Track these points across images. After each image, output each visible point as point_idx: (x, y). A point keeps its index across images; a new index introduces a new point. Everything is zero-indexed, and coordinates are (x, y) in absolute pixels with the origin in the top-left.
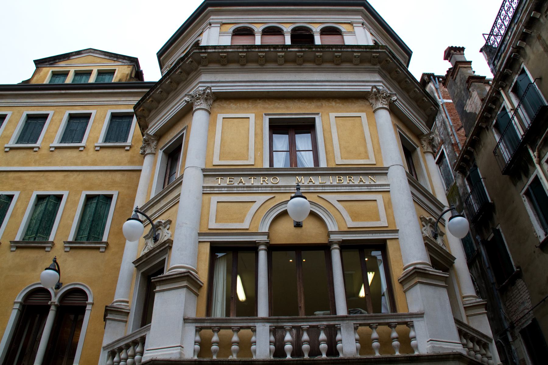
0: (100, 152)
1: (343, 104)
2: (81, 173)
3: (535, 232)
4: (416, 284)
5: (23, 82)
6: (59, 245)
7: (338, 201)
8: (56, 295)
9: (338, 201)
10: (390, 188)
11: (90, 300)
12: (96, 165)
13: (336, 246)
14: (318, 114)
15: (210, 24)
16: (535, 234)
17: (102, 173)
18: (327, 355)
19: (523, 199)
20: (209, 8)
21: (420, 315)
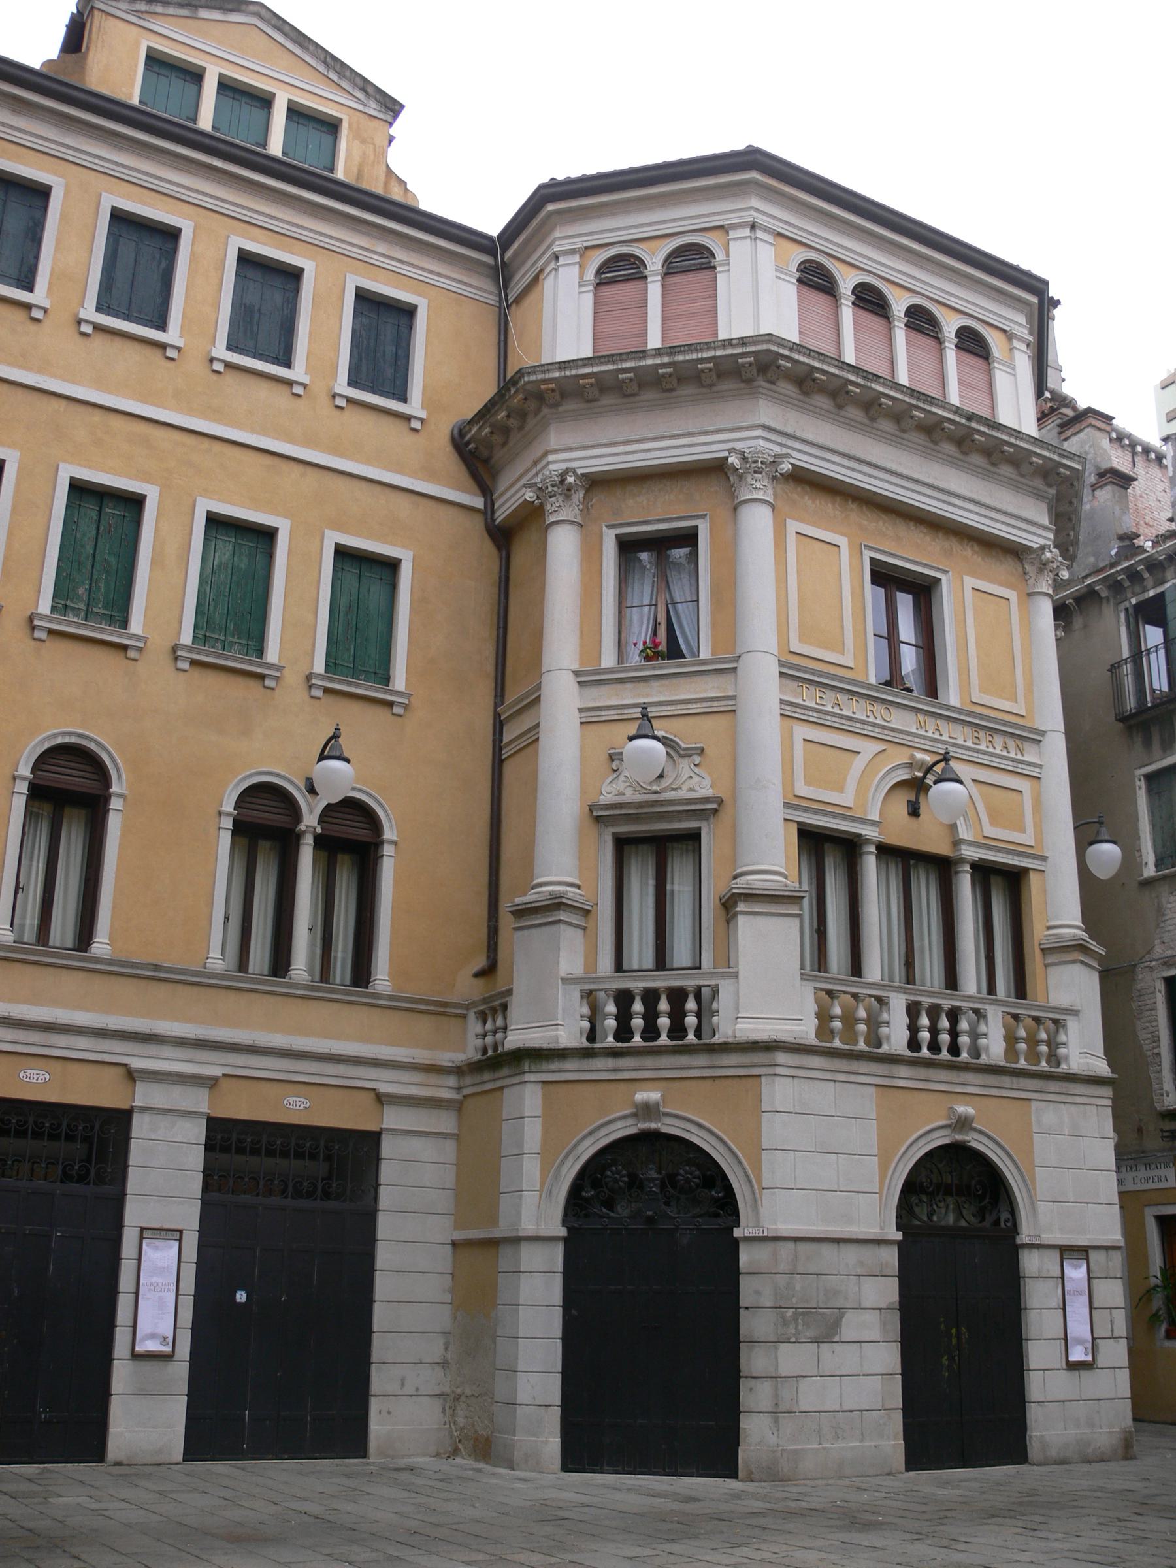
0: (347, 413)
1: (983, 559)
2: (309, 470)
3: (1139, 851)
4: (1074, 962)
6: (293, 678)
7: (974, 780)
8: (311, 811)
9: (974, 780)
10: (1044, 774)
11: (388, 834)
12: (342, 455)
13: (967, 868)
14: (946, 572)
15: (557, 258)
16: (1137, 854)
17: (363, 484)
18: (643, 1038)
19: (1138, 783)
20: (551, 207)
21: (1075, 1013)
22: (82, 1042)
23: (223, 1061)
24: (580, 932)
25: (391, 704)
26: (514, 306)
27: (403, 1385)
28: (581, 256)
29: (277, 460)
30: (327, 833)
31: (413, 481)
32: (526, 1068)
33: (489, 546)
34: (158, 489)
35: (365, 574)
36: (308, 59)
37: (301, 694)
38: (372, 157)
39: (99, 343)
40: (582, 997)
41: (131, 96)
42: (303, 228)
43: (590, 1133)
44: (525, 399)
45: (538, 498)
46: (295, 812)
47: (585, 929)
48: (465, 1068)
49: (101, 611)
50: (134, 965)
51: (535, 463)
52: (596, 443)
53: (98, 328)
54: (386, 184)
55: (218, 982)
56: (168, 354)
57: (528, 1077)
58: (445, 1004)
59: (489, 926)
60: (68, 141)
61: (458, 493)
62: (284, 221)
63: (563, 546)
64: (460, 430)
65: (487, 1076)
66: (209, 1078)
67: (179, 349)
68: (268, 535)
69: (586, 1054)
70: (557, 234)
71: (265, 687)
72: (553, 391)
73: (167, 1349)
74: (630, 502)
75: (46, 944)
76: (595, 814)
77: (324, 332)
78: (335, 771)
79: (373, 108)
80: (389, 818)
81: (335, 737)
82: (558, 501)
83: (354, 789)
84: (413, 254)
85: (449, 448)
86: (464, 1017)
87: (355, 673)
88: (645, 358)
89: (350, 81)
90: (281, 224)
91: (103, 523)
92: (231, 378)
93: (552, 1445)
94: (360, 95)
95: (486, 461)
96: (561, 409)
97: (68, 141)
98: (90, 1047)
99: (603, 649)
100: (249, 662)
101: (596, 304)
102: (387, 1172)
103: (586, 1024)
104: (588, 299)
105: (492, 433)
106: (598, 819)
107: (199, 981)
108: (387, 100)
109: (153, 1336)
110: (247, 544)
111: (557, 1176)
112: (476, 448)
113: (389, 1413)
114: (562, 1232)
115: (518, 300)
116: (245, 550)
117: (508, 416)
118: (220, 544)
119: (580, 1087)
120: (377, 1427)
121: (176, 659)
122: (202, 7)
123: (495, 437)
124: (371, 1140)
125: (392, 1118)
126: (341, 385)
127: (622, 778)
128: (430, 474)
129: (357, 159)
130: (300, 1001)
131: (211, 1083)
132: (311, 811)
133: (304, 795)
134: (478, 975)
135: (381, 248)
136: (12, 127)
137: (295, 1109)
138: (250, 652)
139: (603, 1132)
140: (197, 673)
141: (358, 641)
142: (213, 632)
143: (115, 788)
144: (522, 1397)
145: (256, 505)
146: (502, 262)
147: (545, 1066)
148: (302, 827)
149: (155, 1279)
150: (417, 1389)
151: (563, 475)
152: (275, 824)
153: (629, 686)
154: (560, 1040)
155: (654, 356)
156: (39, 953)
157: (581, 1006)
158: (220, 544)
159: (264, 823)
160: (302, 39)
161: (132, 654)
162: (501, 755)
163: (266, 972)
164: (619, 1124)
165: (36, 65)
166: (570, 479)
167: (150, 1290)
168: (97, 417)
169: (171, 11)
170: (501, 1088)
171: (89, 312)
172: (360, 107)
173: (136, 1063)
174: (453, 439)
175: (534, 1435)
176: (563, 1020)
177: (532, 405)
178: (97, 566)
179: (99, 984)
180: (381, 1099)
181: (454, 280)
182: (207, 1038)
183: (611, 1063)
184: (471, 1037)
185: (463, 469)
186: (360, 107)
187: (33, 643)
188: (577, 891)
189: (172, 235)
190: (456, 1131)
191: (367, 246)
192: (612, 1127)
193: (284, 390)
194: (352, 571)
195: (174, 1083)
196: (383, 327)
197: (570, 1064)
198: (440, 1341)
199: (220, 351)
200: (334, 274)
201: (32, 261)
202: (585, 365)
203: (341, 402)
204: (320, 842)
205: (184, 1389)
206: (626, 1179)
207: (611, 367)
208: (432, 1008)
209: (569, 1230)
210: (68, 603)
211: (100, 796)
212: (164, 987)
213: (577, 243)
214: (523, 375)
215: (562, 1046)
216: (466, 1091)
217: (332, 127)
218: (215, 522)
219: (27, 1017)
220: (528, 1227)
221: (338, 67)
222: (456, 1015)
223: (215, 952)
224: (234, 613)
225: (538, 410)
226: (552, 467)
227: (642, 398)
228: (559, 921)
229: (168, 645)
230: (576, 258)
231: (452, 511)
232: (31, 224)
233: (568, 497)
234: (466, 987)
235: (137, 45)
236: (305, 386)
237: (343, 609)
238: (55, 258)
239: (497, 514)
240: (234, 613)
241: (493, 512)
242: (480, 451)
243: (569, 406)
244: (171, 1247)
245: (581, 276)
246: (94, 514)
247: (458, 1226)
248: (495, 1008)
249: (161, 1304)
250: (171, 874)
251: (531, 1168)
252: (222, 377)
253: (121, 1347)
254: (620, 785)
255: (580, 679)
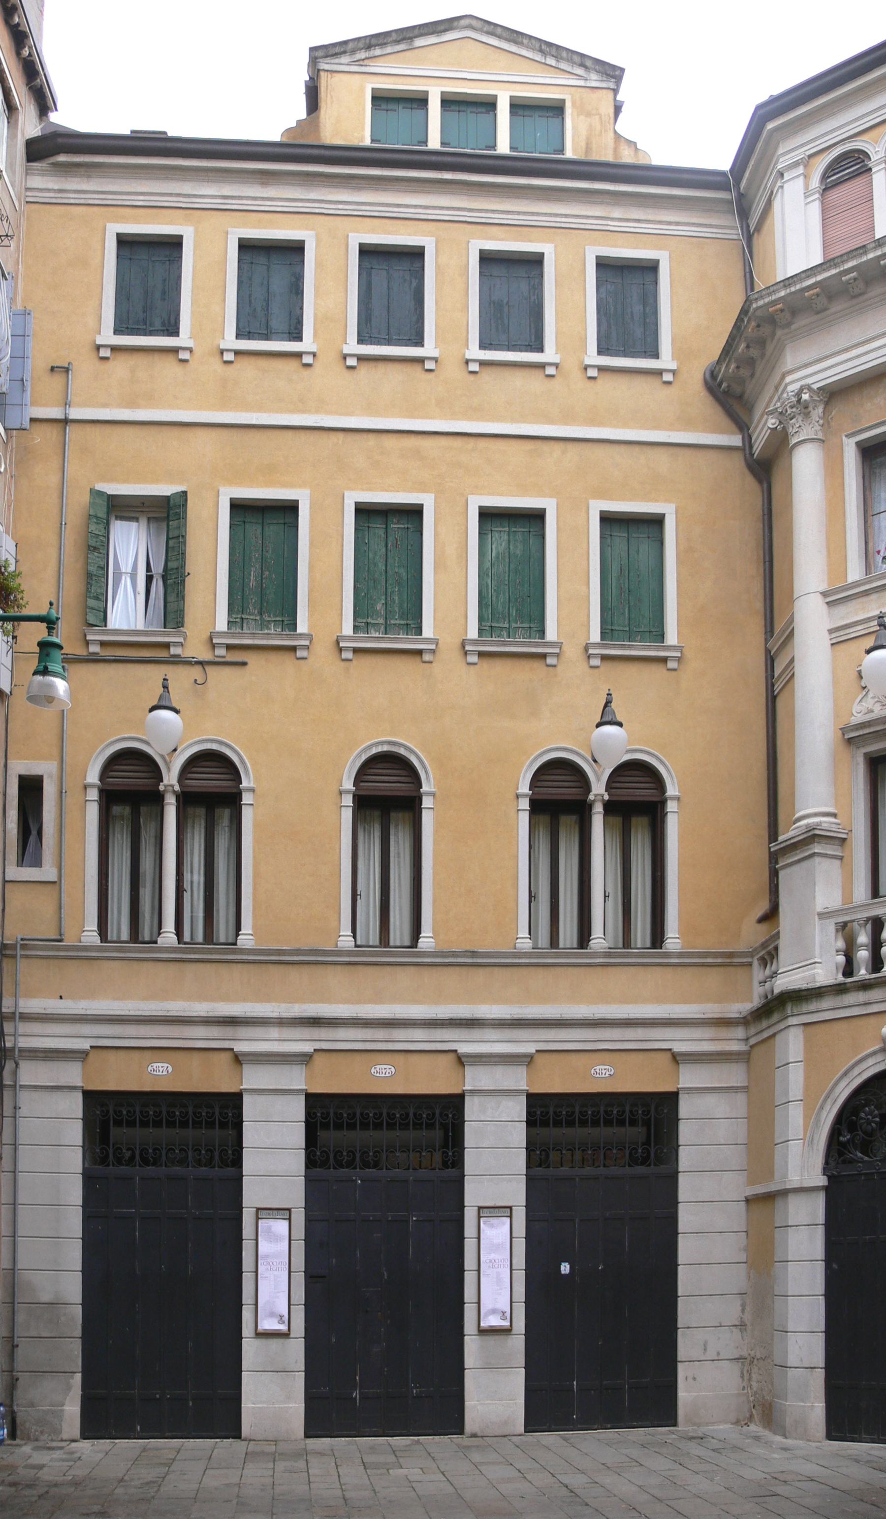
0: (599, 382)
2: (570, 446)
5: (132, 132)
6: (573, 652)
8: (598, 779)
11: (672, 790)
15: (782, 175)
17: (622, 448)
20: (770, 126)
22: (418, 1034)
23: (535, 1038)
24: (837, 863)
25: (664, 660)
26: (756, 235)
27: (705, 1350)
28: (805, 166)
29: (539, 443)
30: (615, 798)
31: (670, 433)
32: (789, 1012)
33: (750, 480)
34: (432, 496)
35: (631, 533)
36: (524, 52)
37: (581, 667)
38: (598, 127)
39: (365, 371)
40: (837, 931)
41: (362, 138)
42: (538, 214)
43: (846, 1074)
44: (758, 326)
45: (780, 423)
46: (585, 783)
47: (841, 858)
48: (749, 1018)
49: (398, 622)
50: (454, 954)
51: (777, 388)
52: (828, 353)
53: (361, 358)
54: (616, 150)
55: (527, 961)
56: (426, 367)
57: (793, 1021)
58: (731, 955)
59: (770, 868)
60: (313, 195)
61: (715, 435)
62: (518, 213)
63: (806, 466)
64: (712, 373)
65: (764, 1023)
66: (525, 1056)
67: (436, 360)
68: (537, 517)
69: (839, 989)
70: (781, 151)
71: (548, 666)
72: (782, 310)
73: (506, 1323)
74: (868, 406)
75: (387, 945)
76: (846, 737)
77: (571, 307)
78: (610, 736)
79: (594, 80)
80: (426, 772)
81: (608, 703)
82: (797, 422)
83: (628, 751)
84: (650, 211)
85: (703, 393)
86: (750, 964)
87: (631, 636)
88: (865, 253)
89: (568, 61)
90: (516, 217)
91: (390, 539)
92: (488, 376)
93: (815, 1409)
94: (580, 71)
95: (740, 397)
96: (793, 327)
97: (313, 195)
98: (425, 1038)
99: (849, 564)
100: (530, 645)
101: (824, 210)
102: (686, 1132)
103: (841, 959)
104: (815, 208)
105: (738, 367)
106: (850, 741)
107: (508, 962)
108: (607, 67)
109: (494, 1311)
110: (520, 530)
111: (818, 1120)
112: (729, 386)
113: (694, 1379)
114: (823, 1181)
115: (758, 229)
116: (519, 537)
117: (748, 347)
118: (496, 535)
119: (837, 1026)
120: (684, 1394)
121: (466, 653)
122: (416, 37)
123: (742, 371)
124: (671, 1099)
125: (688, 1078)
126: (593, 358)
127: (871, 695)
128: (688, 424)
129: (584, 133)
130: (599, 969)
131: (528, 1060)
132: (598, 779)
133: (591, 766)
134: (761, 920)
135: (617, 213)
136: (263, 199)
137: (160, 1075)
138: (533, 634)
139: (856, 1071)
140: (486, 664)
141: (632, 604)
142: (498, 622)
143: (425, 788)
144: (792, 1360)
145: (524, 490)
146: (738, 195)
147: (806, 1008)
148: (591, 797)
149: (493, 1256)
150: (718, 1354)
151: (799, 394)
152: (570, 798)
153: (874, 597)
154: (818, 979)
155: (875, 248)
156: (210, 952)
157: (836, 938)
158: (496, 535)
159: (558, 799)
160: (515, 36)
161: (427, 657)
162: (773, 691)
163: (575, 945)
164: (871, 1061)
165: (276, 138)
166: (805, 397)
167: (489, 1267)
168: (372, 440)
169: (389, 49)
170: (774, 1035)
171: (353, 346)
172: (582, 83)
173: (464, 1049)
174: (706, 383)
175: (802, 1400)
176: (821, 957)
177: (766, 330)
178: (390, 581)
179: (429, 977)
180: (676, 1058)
181: (693, 224)
182: (520, 1016)
183: (861, 997)
184: (756, 984)
185: (719, 410)
186: (582, 83)
187: (342, 664)
188: (832, 820)
189: (416, 254)
190: (746, 1084)
191: (603, 215)
192: (864, 1066)
193: (537, 374)
194: (619, 535)
195: (496, 1064)
196: (627, 287)
197: (827, 1003)
198: (737, 1303)
199: (475, 352)
200: (571, 249)
201: (298, 312)
202: (808, 277)
203: (593, 373)
204: (610, 808)
205: (522, 1361)
206: (878, 1119)
207: (834, 272)
208: (719, 960)
209: (829, 1178)
210: (369, 620)
211: (415, 797)
212: (481, 971)
213: (799, 155)
214: (751, 304)
215: (818, 985)
216: (753, 1041)
217: (556, 109)
218: (487, 515)
219: (371, 1016)
220: (794, 1179)
221: (554, 52)
222: (742, 965)
223: (523, 932)
224: (513, 602)
225: (773, 334)
226: (790, 388)
227: (872, 294)
228: (813, 855)
229: (458, 641)
230: (801, 170)
231: (712, 455)
232: (293, 279)
233: (807, 415)
234: (751, 934)
235: (362, 89)
236: (557, 365)
237: (615, 574)
238: (315, 304)
239: (754, 449)
240: (513, 602)
241: (751, 447)
242: (731, 390)
243: (802, 321)
244: (504, 1224)
245: (806, 186)
246: (382, 533)
247: (751, 1182)
248: (769, 954)
249: (499, 1280)
250: (480, 859)
251: (795, 1116)
252: (479, 375)
253: (469, 1326)
254: (869, 703)
255: (828, 600)
